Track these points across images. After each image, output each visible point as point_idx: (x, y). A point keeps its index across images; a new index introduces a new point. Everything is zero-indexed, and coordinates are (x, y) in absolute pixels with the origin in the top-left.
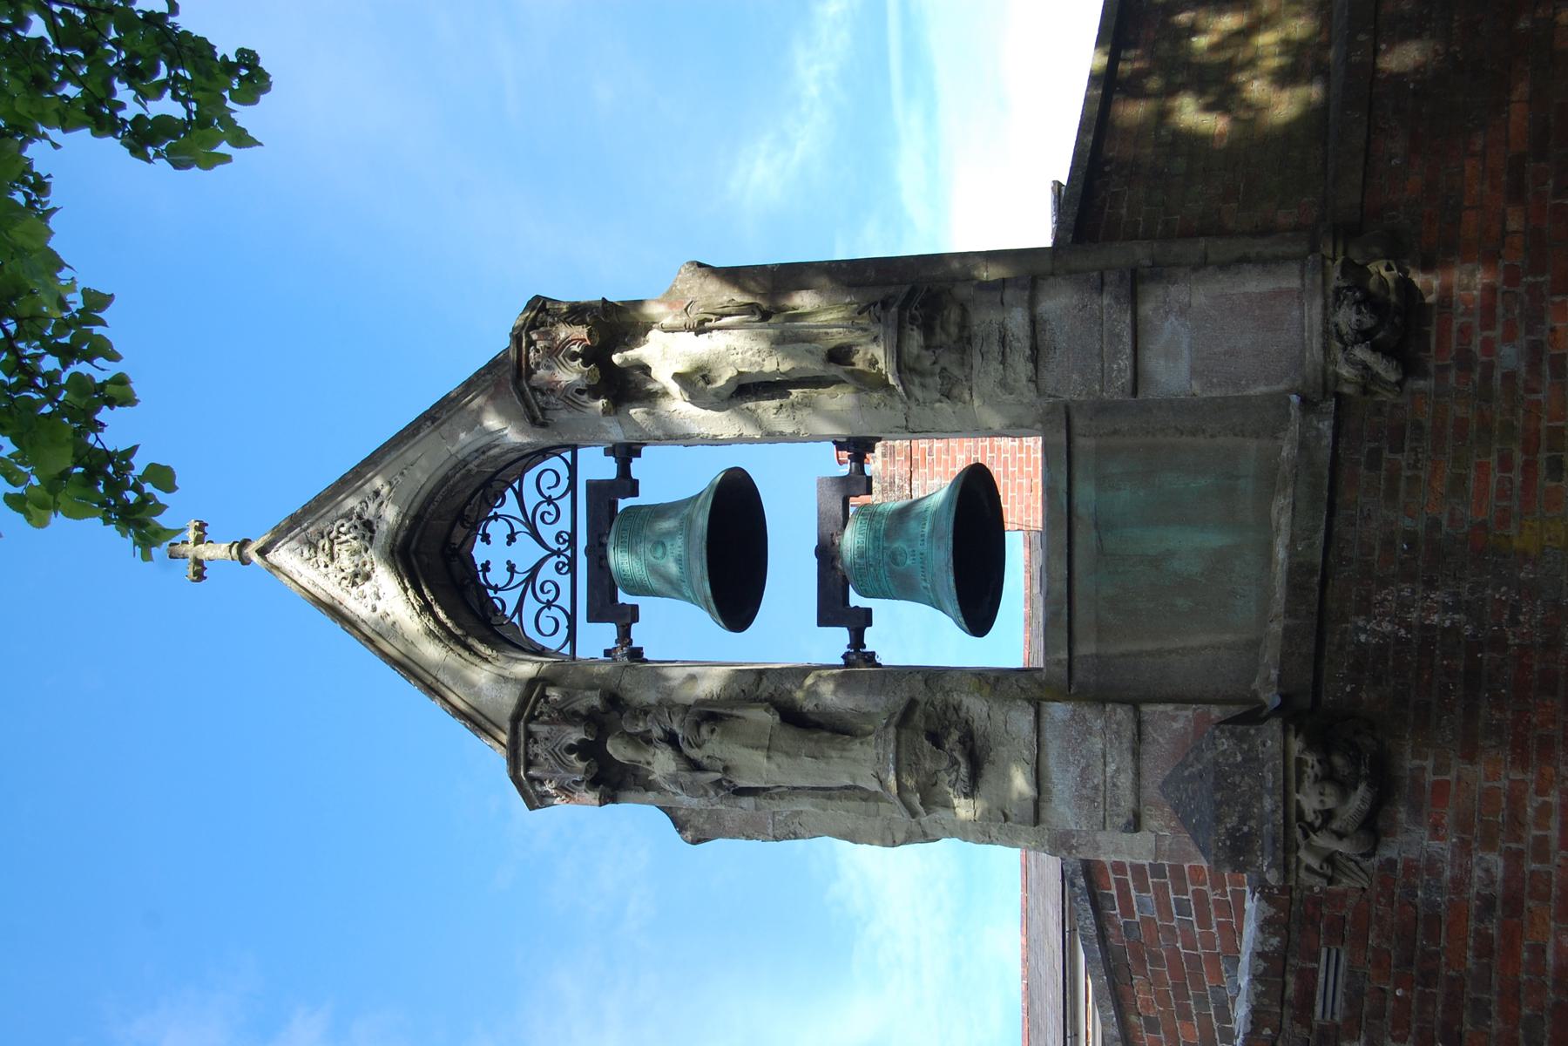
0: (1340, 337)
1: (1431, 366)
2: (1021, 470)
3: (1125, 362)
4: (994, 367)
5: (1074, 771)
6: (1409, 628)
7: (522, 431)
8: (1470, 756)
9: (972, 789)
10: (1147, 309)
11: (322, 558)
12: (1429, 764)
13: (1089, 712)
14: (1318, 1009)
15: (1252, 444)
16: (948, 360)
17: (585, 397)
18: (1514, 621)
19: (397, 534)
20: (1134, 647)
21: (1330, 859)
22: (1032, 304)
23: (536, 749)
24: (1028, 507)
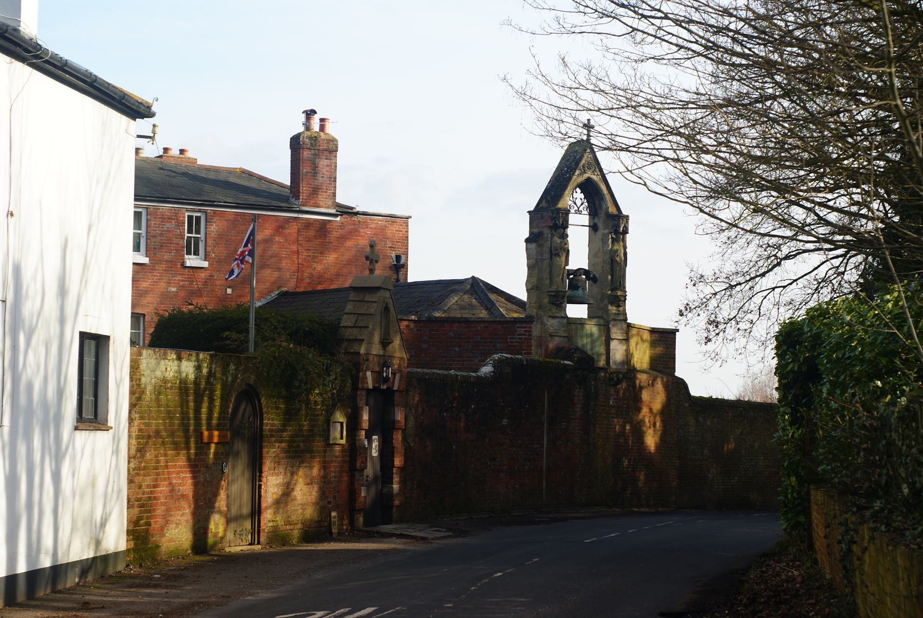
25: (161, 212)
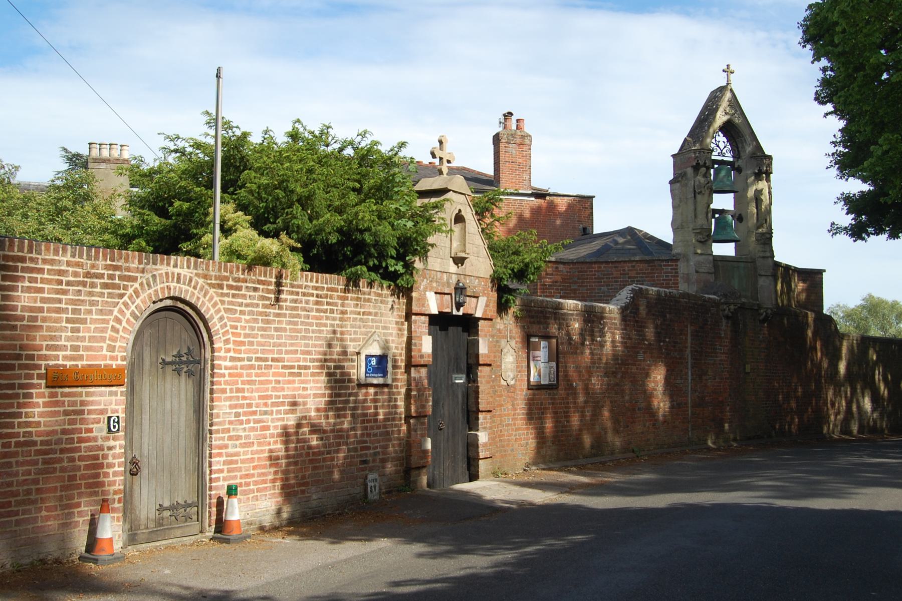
4: (761, 250)
10: (770, 278)
16: (762, 241)
21: (724, 310)
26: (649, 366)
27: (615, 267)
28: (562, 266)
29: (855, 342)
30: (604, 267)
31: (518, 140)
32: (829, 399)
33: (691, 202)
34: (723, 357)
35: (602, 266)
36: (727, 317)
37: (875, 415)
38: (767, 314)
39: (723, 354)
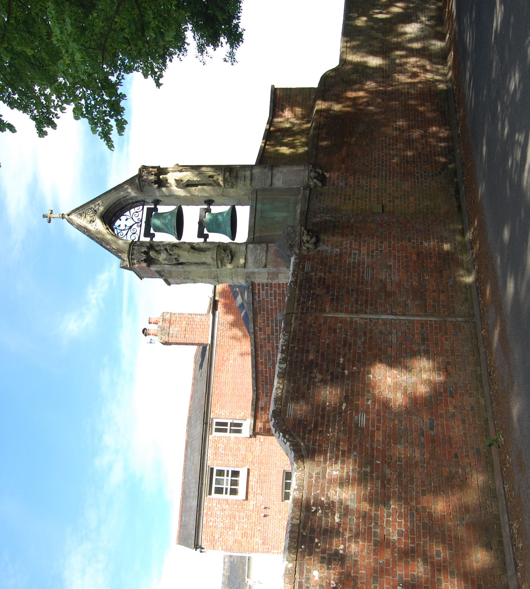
0: (311, 178)
1: (328, 185)
2: (200, 327)
3: (269, 181)
4: (243, 182)
5: (253, 257)
6: (323, 220)
7: (135, 193)
8: (333, 236)
9: (230, 263)
10: (274, 172)
11: (83, 218)
12: (326, 237)
13: (257, 246)
14: (306, 269)
15: (293, 198)
16: (233, 180)
17: (153, 184)
18: (342, 219)
19: (102, 213)
20: (267, 234)
21: (308, 248)
22: (251, 170)
23: (135, 252)
24: (201, 337)
25: (212, 455)
26: (375, 400)
27: (261, 347)
28: (260, 402)
29: (348, 45)
30: (261, 358)
31: (167, 325)
32: (409, 80)
33: (187, 268)
34: (364, 250)
35: (260, 361)
36: (316, 244)
37: (423, 19)
38: (315, 178)
39: (360, 251)
